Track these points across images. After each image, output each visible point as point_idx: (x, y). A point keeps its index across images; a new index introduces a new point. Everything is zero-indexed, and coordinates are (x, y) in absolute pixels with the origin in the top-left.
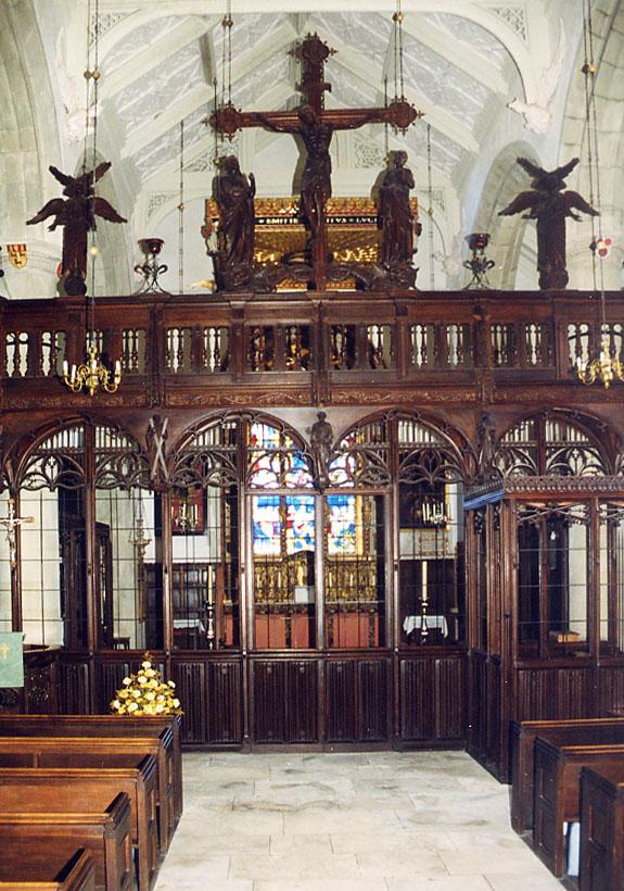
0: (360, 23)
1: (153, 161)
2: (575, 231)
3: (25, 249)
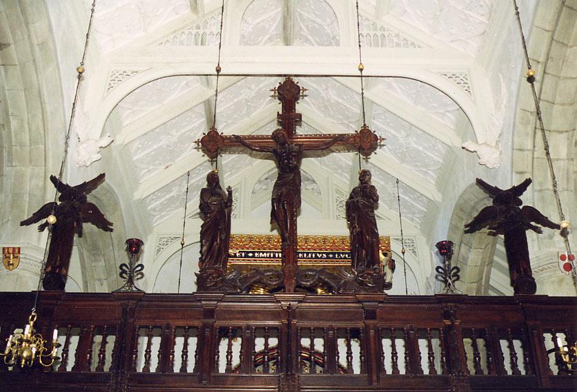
0: (336, 98)
1: (164, 207)
2: (536, 249)
3: (19, 252)
